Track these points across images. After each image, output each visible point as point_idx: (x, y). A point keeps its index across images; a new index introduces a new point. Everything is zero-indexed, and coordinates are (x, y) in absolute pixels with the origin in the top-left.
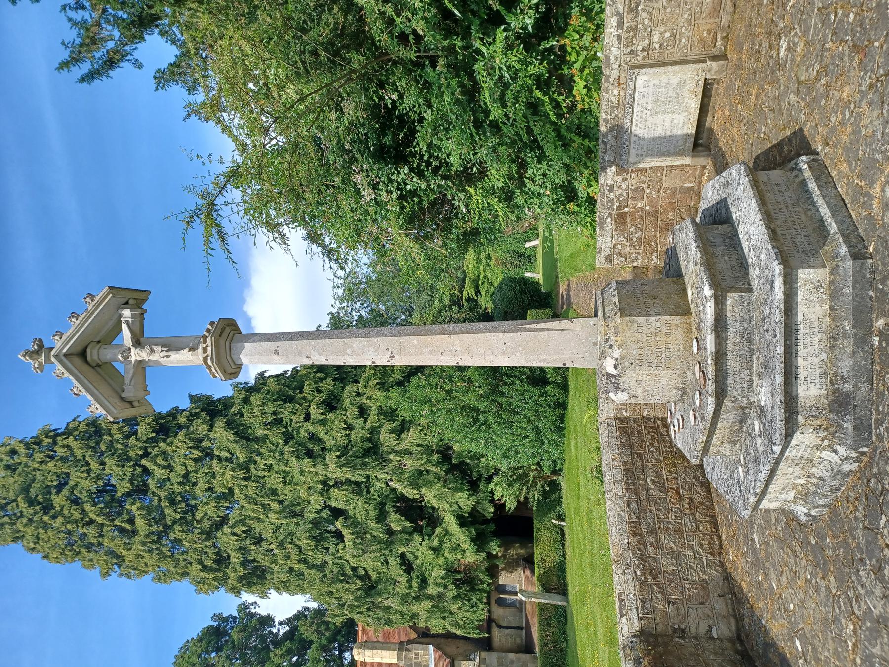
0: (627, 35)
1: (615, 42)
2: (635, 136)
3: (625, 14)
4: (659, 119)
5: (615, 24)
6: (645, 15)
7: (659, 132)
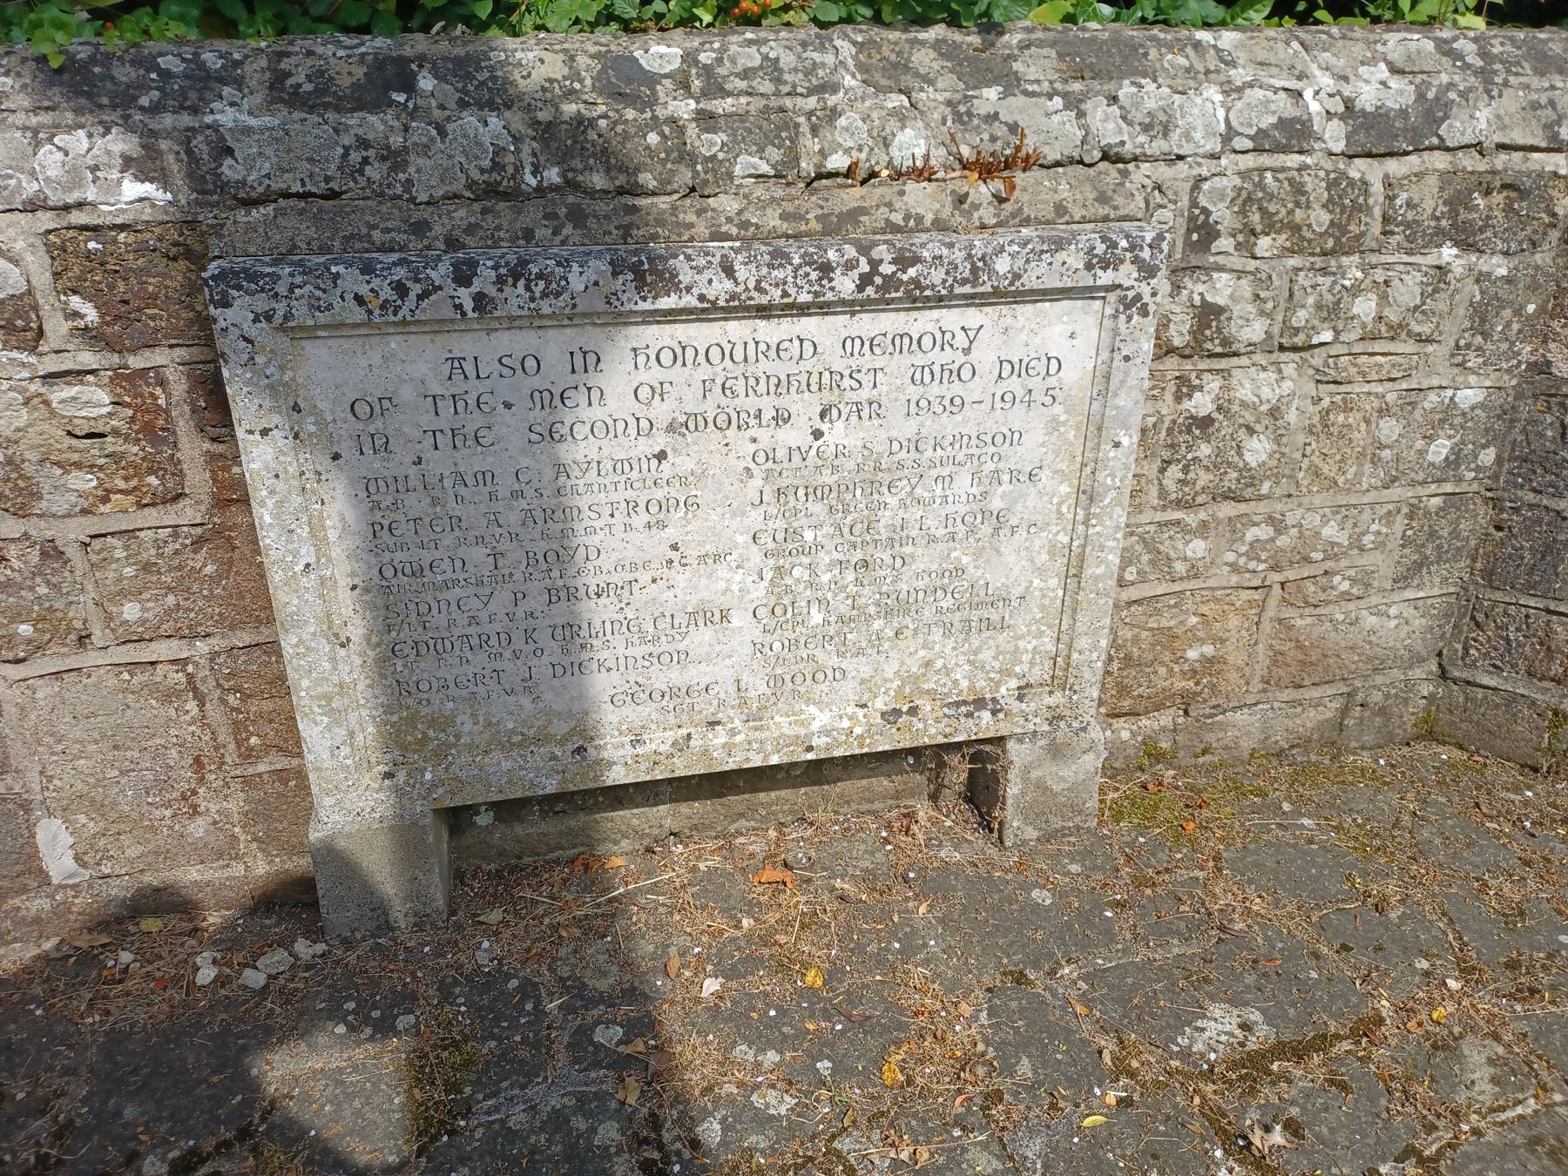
0: (1315, 187)
1: (1263, 108)
2: (587, 360)
3: (1440, 161)
4: (730, 520)
5: (1368, 96)
6: (1407, 290)
7: (609, 542)
